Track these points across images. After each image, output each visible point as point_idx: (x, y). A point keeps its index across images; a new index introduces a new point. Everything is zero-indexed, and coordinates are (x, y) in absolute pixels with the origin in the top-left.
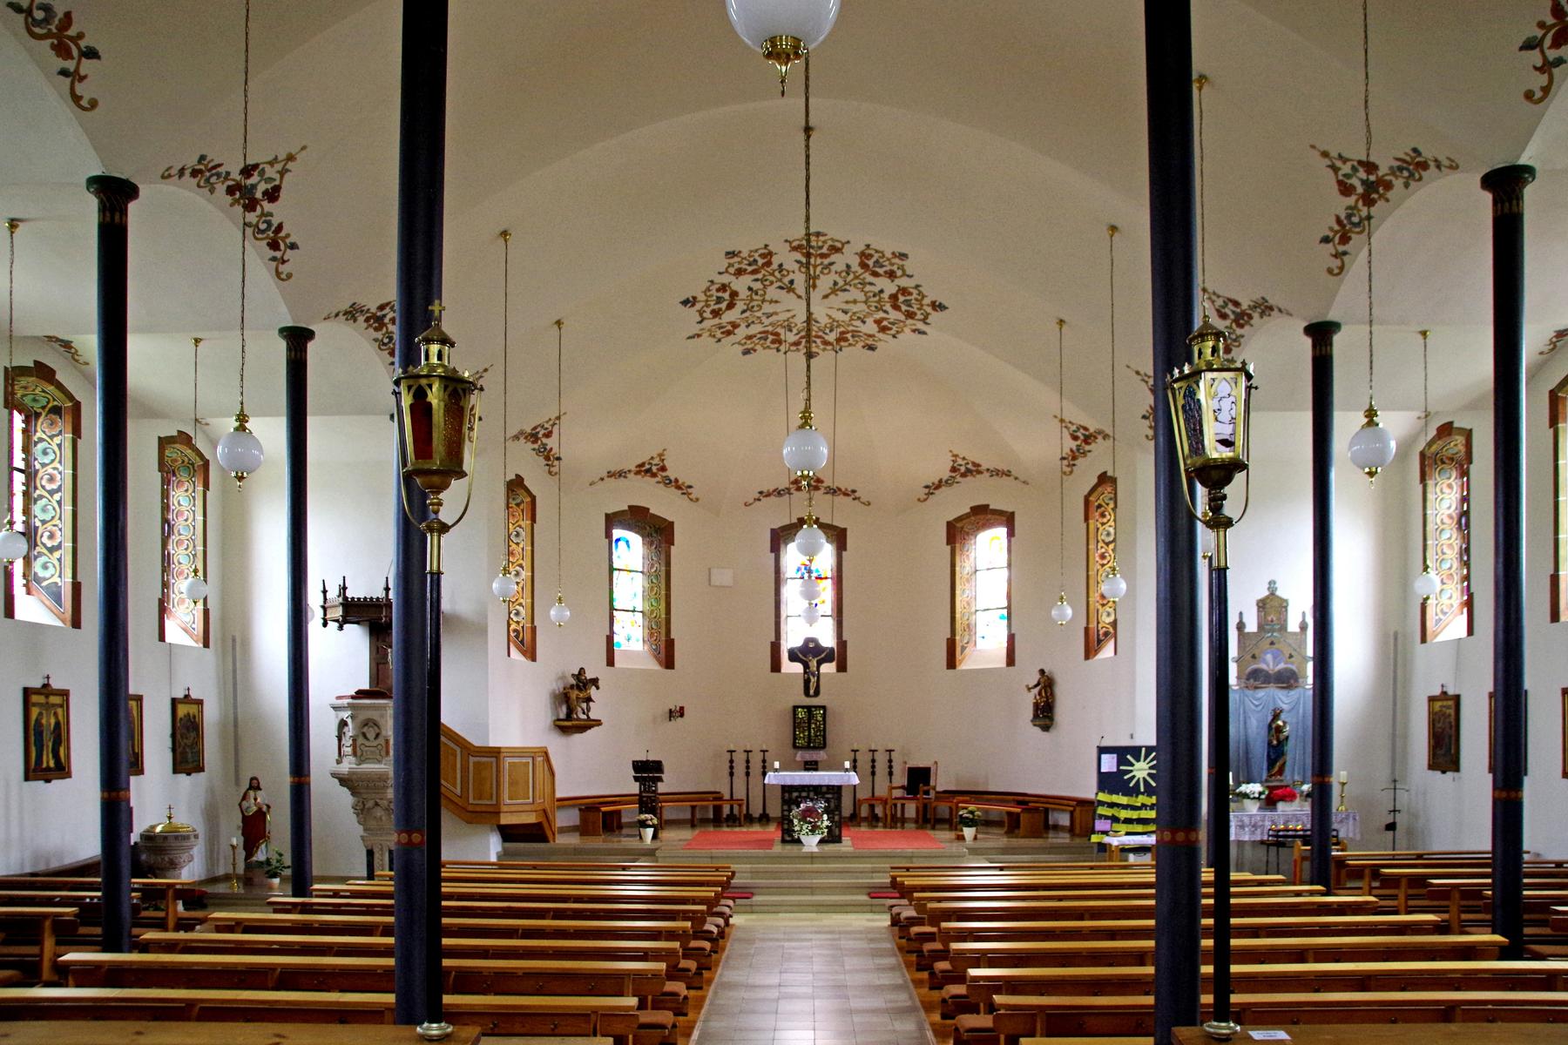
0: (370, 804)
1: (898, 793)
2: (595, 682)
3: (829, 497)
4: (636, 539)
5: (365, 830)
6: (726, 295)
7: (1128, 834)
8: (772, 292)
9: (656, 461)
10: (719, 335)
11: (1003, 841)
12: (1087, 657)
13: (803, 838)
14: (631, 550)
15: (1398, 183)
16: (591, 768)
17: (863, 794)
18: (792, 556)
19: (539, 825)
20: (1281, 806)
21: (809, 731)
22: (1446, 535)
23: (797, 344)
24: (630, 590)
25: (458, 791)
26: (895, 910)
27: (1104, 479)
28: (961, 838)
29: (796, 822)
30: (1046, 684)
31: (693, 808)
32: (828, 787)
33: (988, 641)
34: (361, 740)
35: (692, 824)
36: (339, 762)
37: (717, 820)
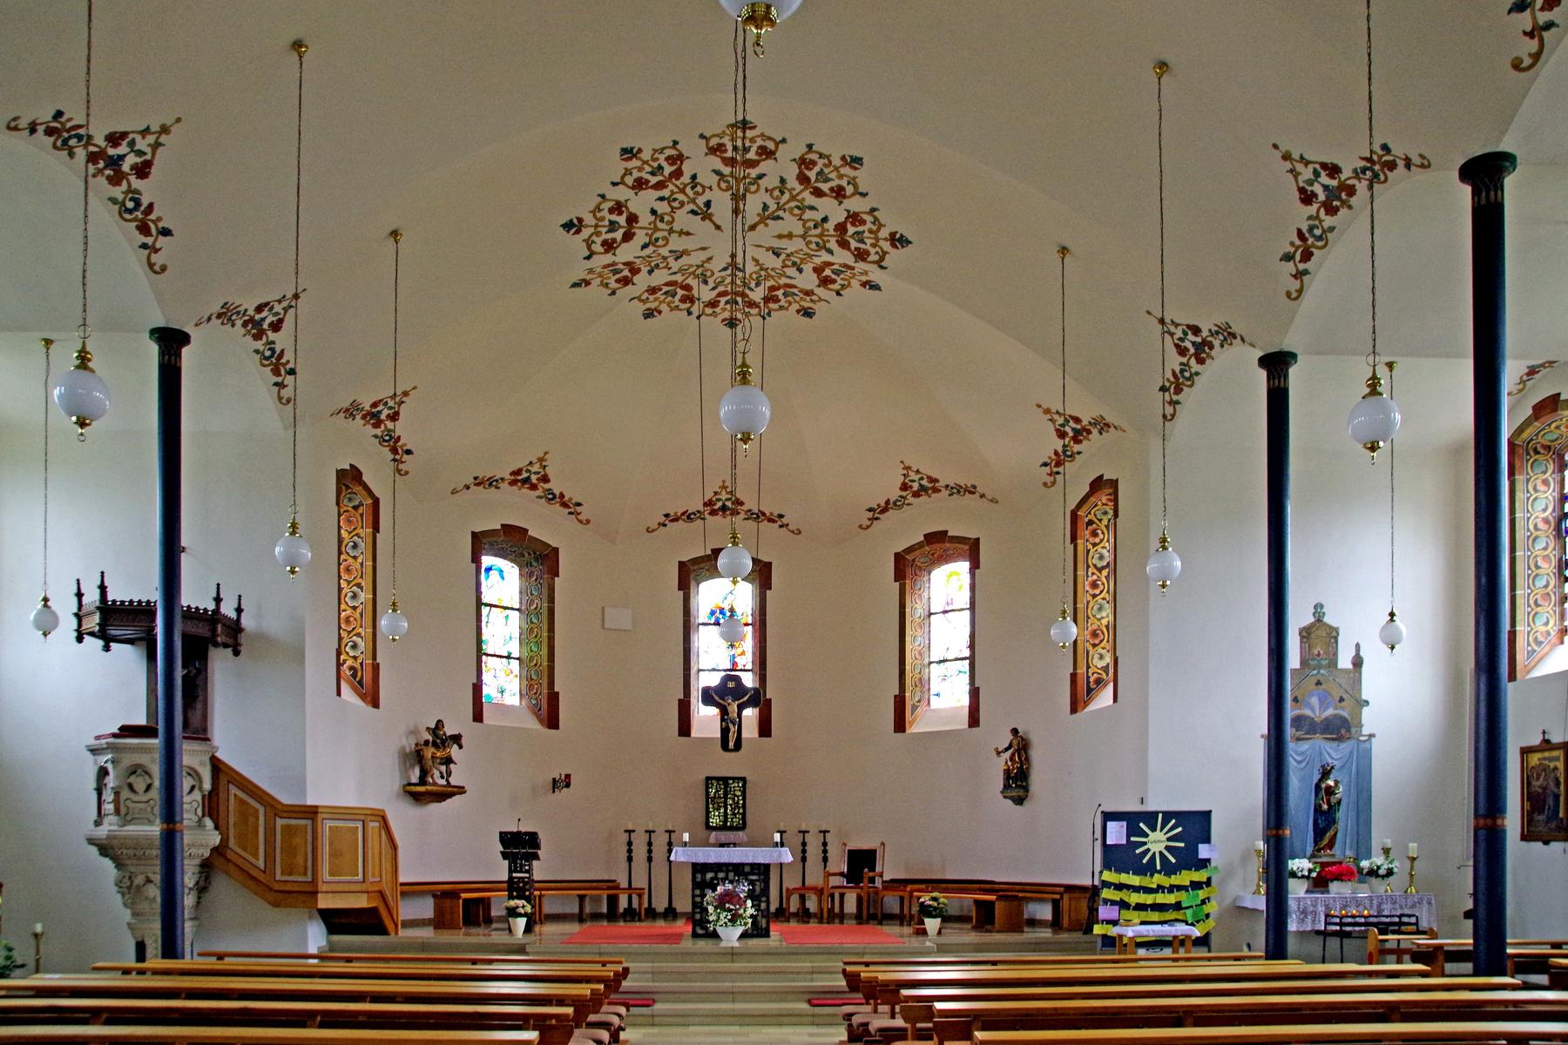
0: (139, 880)
1: (835, 881)
2: (457, 739)
3: (752, 524)
4: (512, 571)
5: (135, 914)
6: (622, 220)
7: (1143, 923)
8: (683, 219)
9: (536, 468)
10: (614, 285)
11: (972, 937)
12: (1074, 710)
13: (720, 930)
14: (503, 582)
15: (1361, 187)
16: (447, 846)
17: (792, 882)
18: (710, 594)
19: (373, 912)
20: (1335, 887)
21: (726, 802)
22: (1540, 544)
23: (713, 304)
24: (503, 632)
25: (261, 864)
26: (856, 1020)
27: (1097, 484)
28: (924, 932)
29: (711, 909)
30: (1021, 747)
31: (582, 898)
32: (753, 865)
33: (948, 693)
34: (125, 794)
35: (580, 918)
36: (98, 823)
37: (612, 915)
